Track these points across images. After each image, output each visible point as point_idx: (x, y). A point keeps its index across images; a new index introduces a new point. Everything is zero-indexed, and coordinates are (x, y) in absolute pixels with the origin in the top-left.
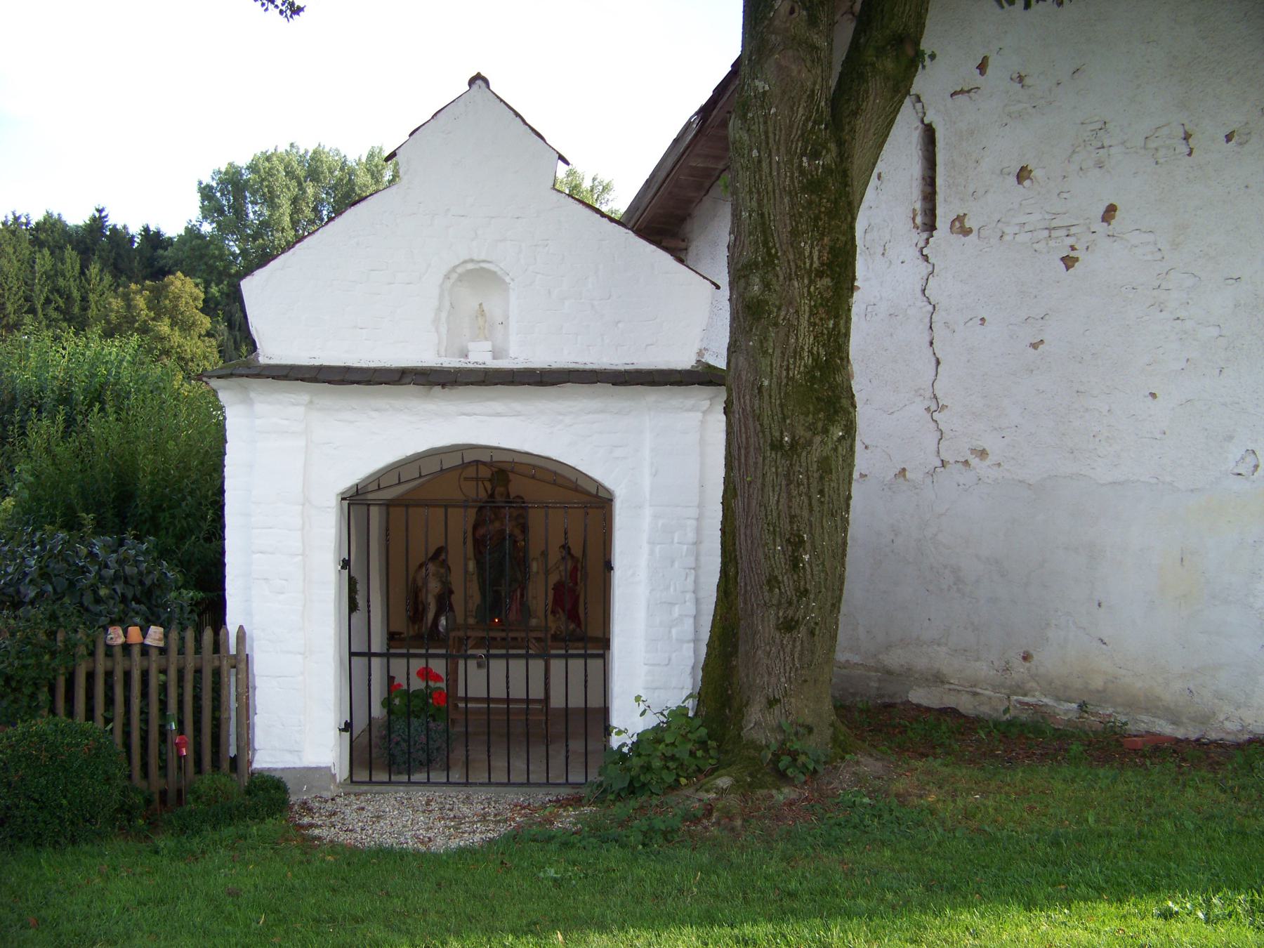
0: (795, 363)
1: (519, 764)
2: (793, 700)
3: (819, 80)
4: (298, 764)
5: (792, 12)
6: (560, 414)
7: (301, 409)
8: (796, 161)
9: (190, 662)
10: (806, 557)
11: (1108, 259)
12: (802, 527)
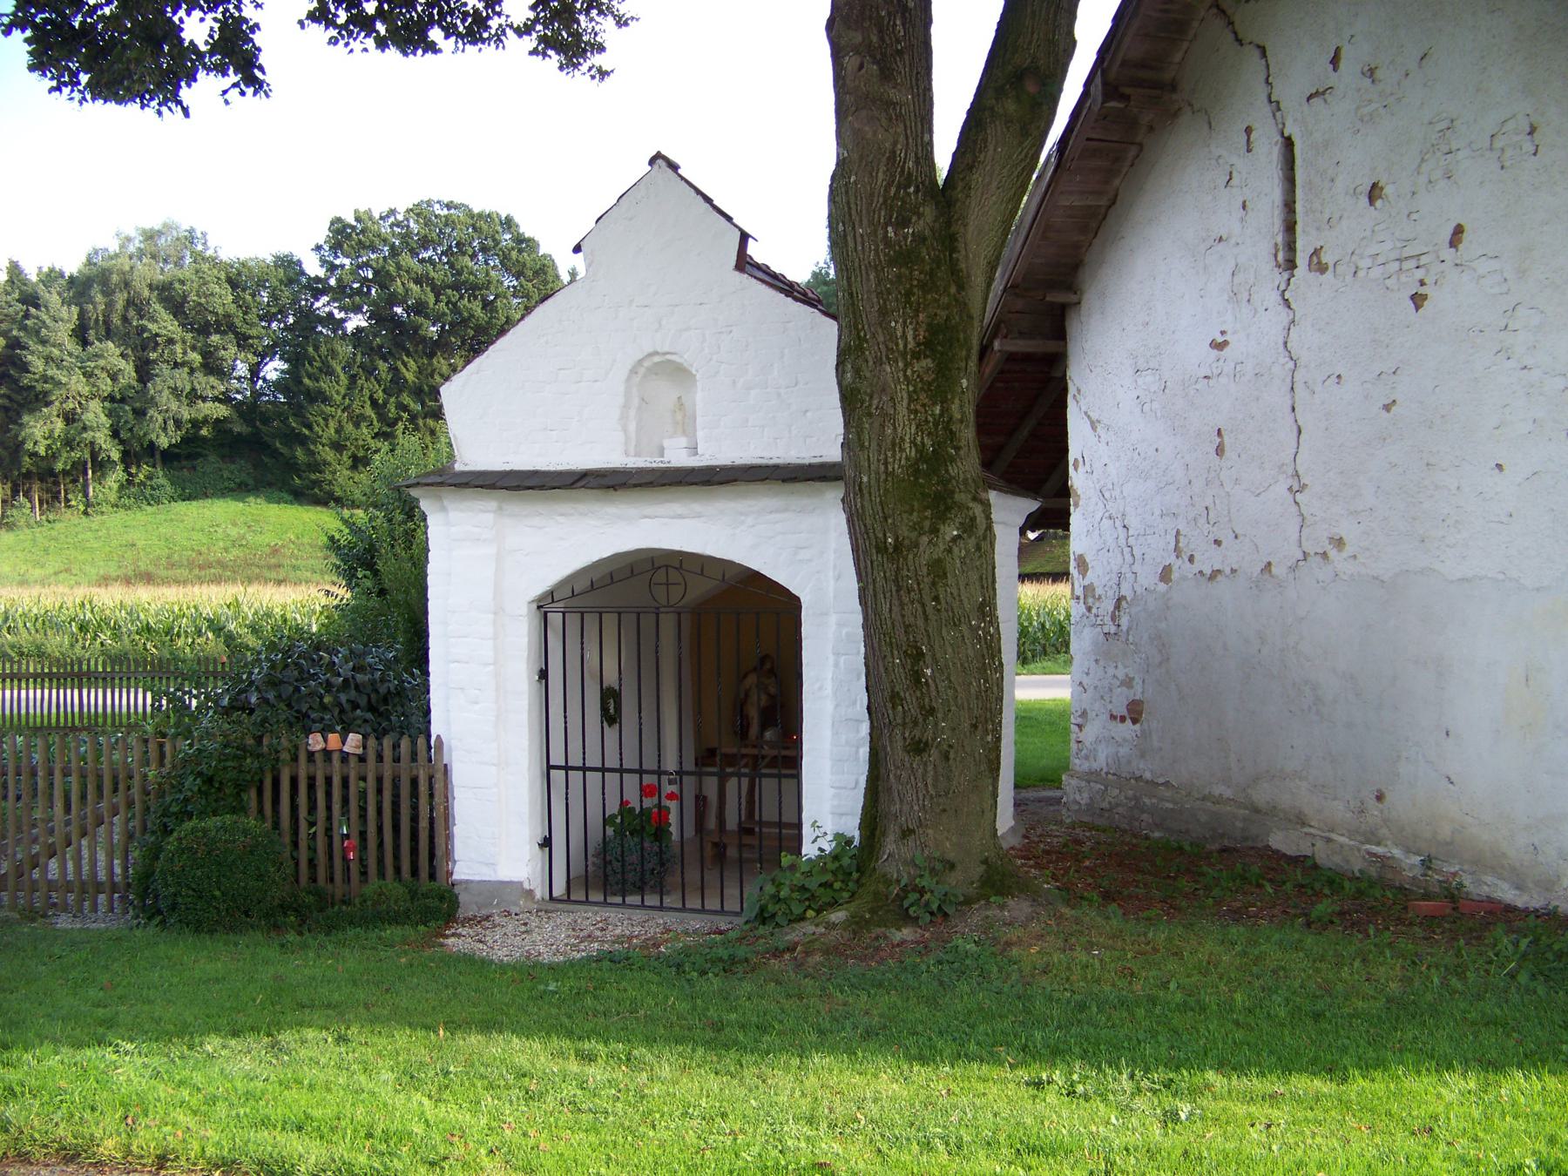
0: (894, 456)
1: (732, 891)
2: (930, 831)
3: (902, 138)
4: (493, 878)
5: (861, 67)
6: (741, 514)
7: (491, 516)
8: (880, 232)
9: (387, 770)
10: (929, 672)
11: (1461, 295)
12: (919, 637)
